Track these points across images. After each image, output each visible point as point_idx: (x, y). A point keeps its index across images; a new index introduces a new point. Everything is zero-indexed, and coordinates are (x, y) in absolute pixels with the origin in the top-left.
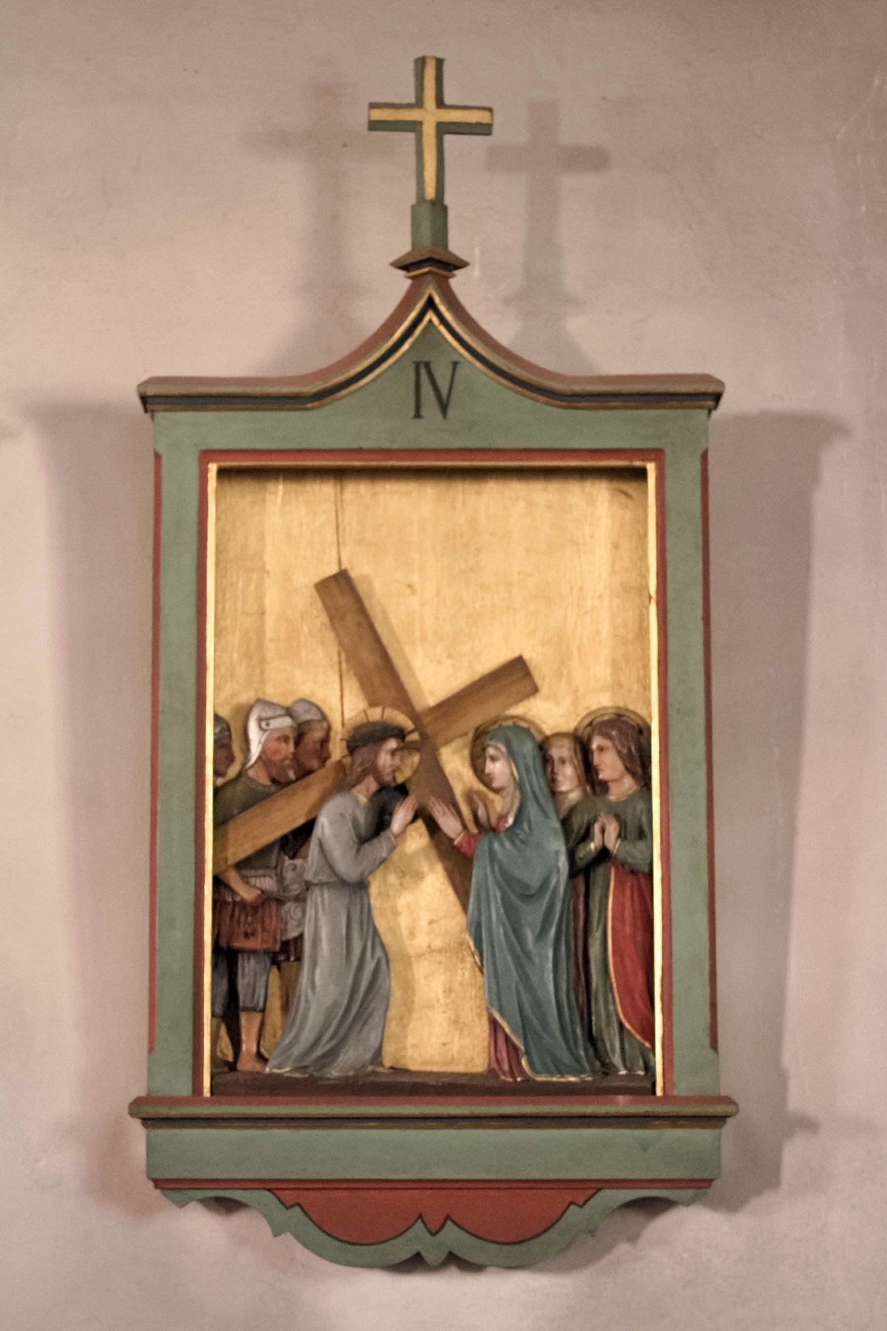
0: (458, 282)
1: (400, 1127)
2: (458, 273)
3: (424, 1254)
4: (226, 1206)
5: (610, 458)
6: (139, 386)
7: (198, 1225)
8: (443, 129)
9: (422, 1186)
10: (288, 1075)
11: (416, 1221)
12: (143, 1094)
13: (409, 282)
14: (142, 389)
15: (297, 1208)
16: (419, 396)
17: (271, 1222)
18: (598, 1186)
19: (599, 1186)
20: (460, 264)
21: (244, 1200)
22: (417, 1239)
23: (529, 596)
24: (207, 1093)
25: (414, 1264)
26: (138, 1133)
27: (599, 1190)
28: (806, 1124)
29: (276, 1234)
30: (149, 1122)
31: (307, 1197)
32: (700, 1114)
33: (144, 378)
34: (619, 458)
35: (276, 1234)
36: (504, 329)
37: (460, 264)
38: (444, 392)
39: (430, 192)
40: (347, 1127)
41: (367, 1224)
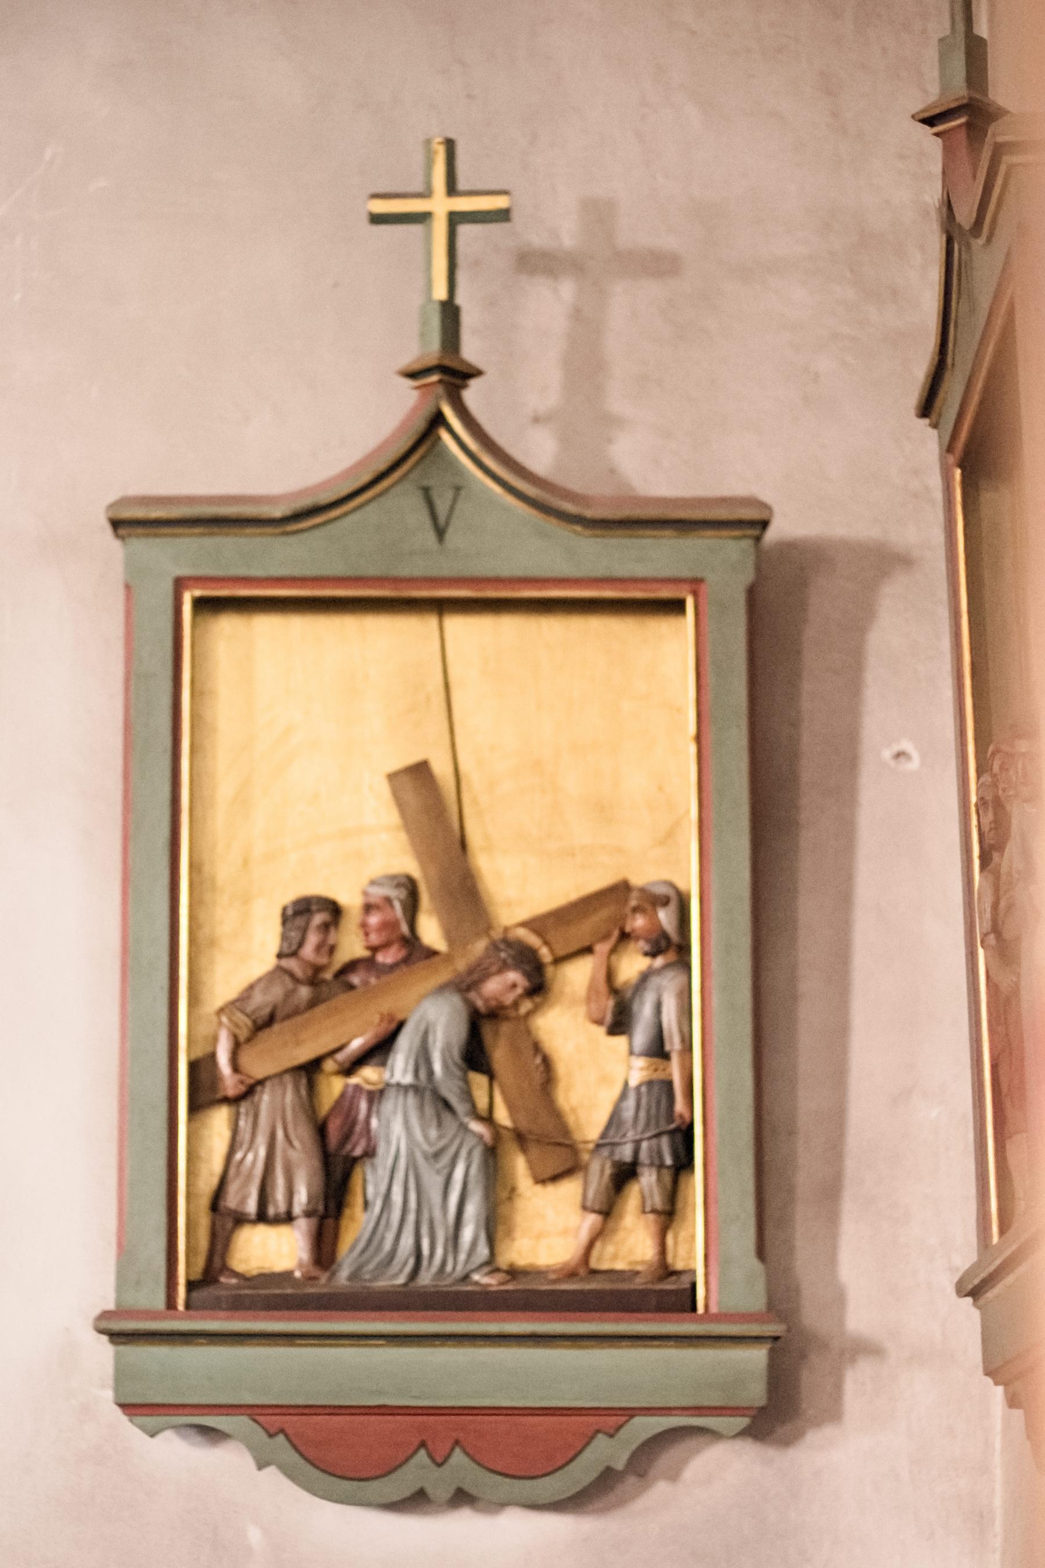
0: (472, 395)
1: (263, 1345)
2: (474, 383)
3: (429, 1490)
4: (211, 1435)
5: (323, 587)
6: (111, 507)
7: (172, 1451)
8: (455, 219)
9: (360, 1411)
10: (454, 1288)
11: (452, 1449)
12: (111, 1306)
13: (415, 394)
14: (111, 514)
15: (281, 1438)
16: (414, 525)
17: (252, 1449)
18: (631, 1413)
19: (631, 1412)
20: (477, 373)
21: (720, 1430)
22: (418, 1472)
23: (588, 756)
24: (181, 1307)
25: (417, 1501)
26: (104, 1350)
27: (632, 1416)
28: (865, 1349)
29: (260, 1467)
30: (117, 1337)
31: (291, 1422)
32: (409, 1333)
33: (112, 498)
34: (382, 587)
35: (260, 1467)
36: (540, 452)
37: (477, 373)
38: (442, 519)
39: (440, 292)
40: (558, 1347)
41: (349, 1452)
